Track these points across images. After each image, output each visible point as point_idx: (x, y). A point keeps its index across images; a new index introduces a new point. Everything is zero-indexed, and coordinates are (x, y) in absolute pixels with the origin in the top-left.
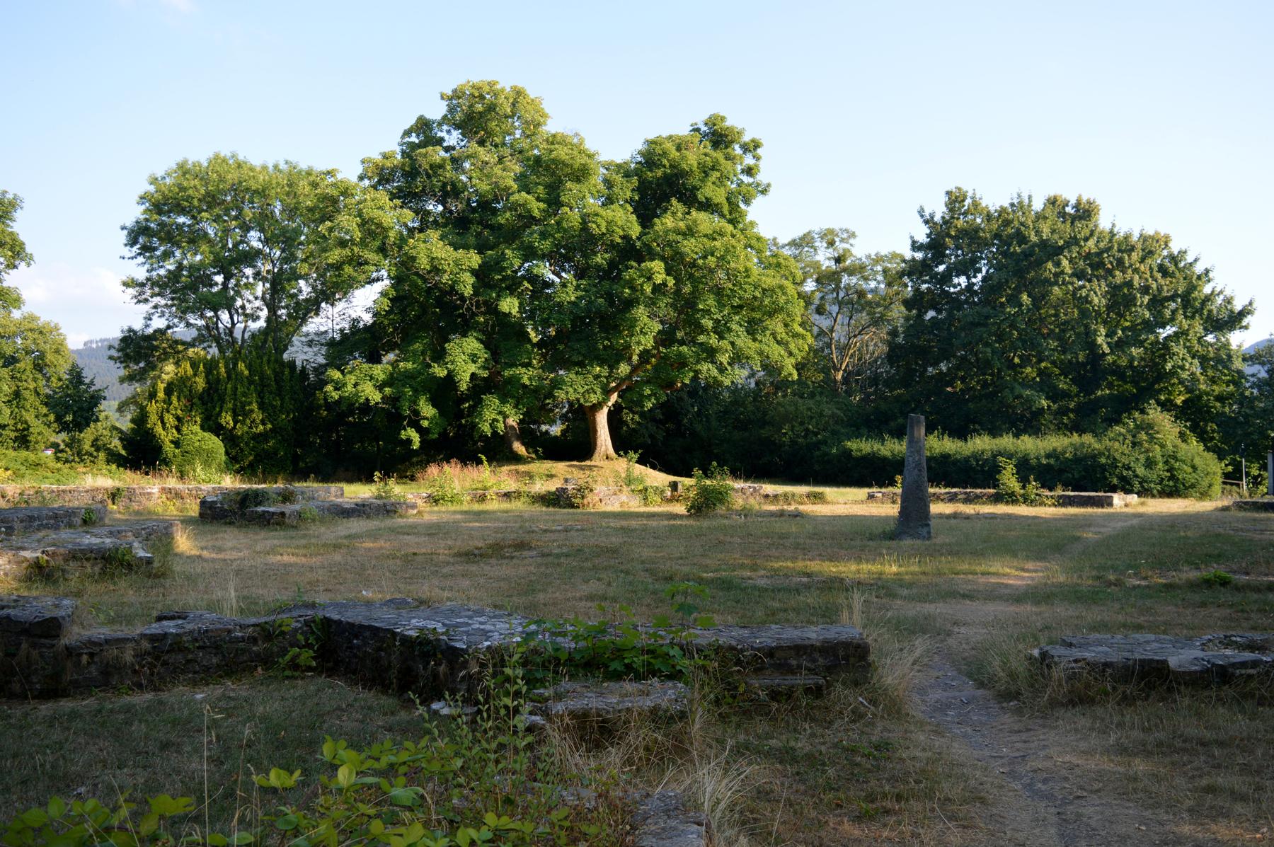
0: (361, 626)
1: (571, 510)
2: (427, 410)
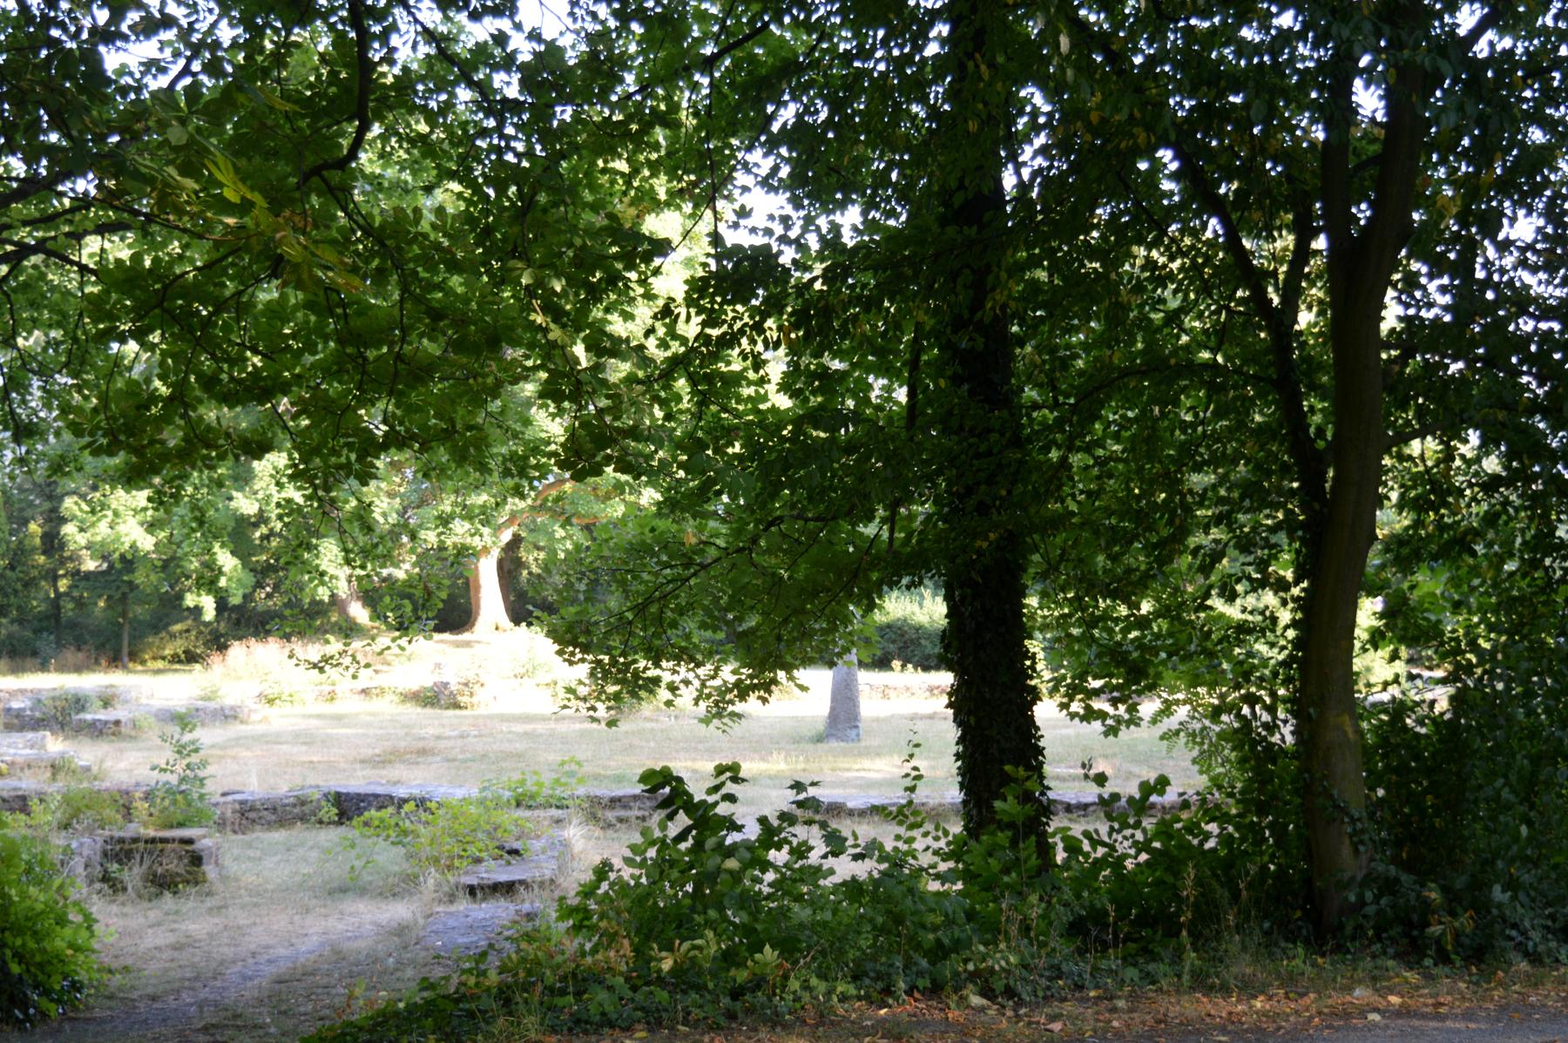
0: (367, 795)
1: (458, 712)
2: (227, 560)
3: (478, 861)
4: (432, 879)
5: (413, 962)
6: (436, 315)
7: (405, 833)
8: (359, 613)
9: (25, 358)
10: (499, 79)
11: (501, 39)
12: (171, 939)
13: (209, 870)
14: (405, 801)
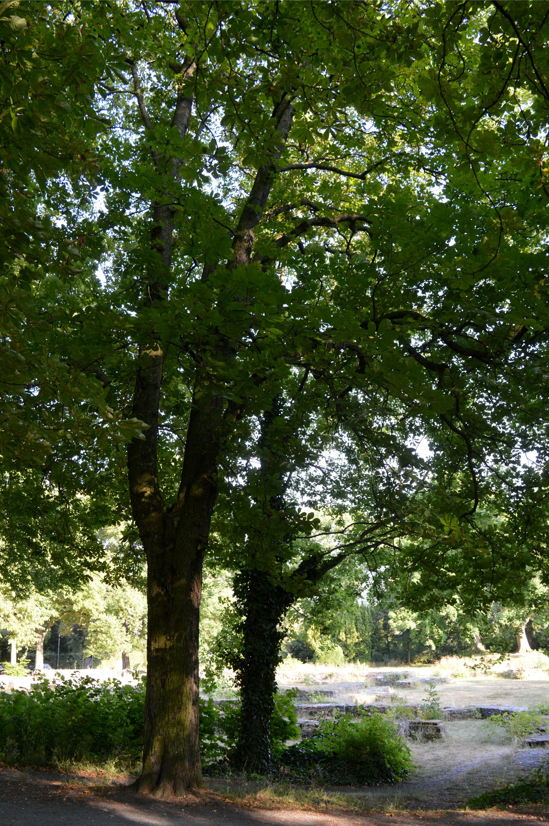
3: (531, 733)
4: (516, 739)
5: (513, 769)
6: (504, 558)
7: (505, 723)
8: (481, 647)
9: (380, 574)
10: (515, 481)
11: (514, 469)
12: (432, 757)
13: (442, 733)
14: (504, 712)
